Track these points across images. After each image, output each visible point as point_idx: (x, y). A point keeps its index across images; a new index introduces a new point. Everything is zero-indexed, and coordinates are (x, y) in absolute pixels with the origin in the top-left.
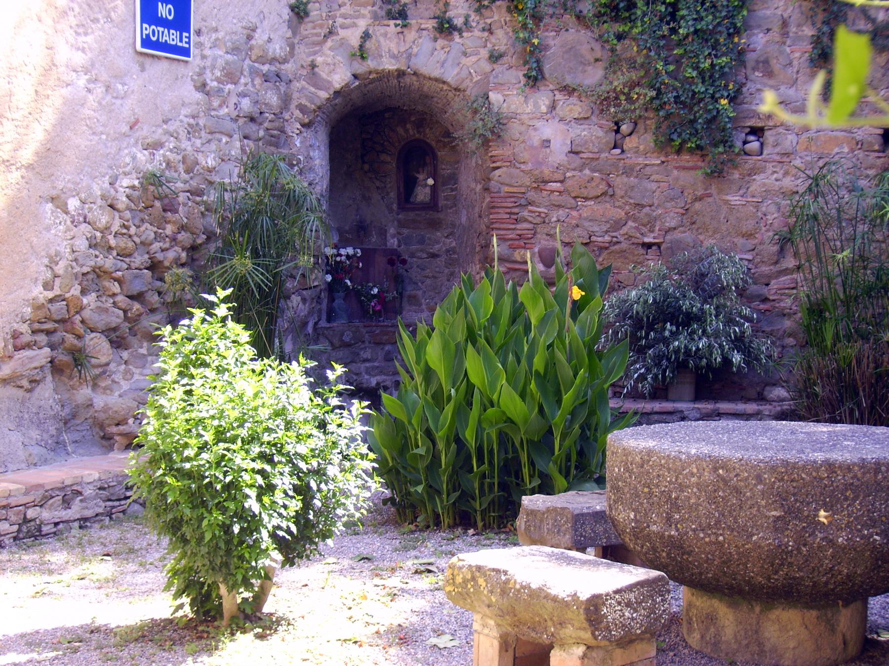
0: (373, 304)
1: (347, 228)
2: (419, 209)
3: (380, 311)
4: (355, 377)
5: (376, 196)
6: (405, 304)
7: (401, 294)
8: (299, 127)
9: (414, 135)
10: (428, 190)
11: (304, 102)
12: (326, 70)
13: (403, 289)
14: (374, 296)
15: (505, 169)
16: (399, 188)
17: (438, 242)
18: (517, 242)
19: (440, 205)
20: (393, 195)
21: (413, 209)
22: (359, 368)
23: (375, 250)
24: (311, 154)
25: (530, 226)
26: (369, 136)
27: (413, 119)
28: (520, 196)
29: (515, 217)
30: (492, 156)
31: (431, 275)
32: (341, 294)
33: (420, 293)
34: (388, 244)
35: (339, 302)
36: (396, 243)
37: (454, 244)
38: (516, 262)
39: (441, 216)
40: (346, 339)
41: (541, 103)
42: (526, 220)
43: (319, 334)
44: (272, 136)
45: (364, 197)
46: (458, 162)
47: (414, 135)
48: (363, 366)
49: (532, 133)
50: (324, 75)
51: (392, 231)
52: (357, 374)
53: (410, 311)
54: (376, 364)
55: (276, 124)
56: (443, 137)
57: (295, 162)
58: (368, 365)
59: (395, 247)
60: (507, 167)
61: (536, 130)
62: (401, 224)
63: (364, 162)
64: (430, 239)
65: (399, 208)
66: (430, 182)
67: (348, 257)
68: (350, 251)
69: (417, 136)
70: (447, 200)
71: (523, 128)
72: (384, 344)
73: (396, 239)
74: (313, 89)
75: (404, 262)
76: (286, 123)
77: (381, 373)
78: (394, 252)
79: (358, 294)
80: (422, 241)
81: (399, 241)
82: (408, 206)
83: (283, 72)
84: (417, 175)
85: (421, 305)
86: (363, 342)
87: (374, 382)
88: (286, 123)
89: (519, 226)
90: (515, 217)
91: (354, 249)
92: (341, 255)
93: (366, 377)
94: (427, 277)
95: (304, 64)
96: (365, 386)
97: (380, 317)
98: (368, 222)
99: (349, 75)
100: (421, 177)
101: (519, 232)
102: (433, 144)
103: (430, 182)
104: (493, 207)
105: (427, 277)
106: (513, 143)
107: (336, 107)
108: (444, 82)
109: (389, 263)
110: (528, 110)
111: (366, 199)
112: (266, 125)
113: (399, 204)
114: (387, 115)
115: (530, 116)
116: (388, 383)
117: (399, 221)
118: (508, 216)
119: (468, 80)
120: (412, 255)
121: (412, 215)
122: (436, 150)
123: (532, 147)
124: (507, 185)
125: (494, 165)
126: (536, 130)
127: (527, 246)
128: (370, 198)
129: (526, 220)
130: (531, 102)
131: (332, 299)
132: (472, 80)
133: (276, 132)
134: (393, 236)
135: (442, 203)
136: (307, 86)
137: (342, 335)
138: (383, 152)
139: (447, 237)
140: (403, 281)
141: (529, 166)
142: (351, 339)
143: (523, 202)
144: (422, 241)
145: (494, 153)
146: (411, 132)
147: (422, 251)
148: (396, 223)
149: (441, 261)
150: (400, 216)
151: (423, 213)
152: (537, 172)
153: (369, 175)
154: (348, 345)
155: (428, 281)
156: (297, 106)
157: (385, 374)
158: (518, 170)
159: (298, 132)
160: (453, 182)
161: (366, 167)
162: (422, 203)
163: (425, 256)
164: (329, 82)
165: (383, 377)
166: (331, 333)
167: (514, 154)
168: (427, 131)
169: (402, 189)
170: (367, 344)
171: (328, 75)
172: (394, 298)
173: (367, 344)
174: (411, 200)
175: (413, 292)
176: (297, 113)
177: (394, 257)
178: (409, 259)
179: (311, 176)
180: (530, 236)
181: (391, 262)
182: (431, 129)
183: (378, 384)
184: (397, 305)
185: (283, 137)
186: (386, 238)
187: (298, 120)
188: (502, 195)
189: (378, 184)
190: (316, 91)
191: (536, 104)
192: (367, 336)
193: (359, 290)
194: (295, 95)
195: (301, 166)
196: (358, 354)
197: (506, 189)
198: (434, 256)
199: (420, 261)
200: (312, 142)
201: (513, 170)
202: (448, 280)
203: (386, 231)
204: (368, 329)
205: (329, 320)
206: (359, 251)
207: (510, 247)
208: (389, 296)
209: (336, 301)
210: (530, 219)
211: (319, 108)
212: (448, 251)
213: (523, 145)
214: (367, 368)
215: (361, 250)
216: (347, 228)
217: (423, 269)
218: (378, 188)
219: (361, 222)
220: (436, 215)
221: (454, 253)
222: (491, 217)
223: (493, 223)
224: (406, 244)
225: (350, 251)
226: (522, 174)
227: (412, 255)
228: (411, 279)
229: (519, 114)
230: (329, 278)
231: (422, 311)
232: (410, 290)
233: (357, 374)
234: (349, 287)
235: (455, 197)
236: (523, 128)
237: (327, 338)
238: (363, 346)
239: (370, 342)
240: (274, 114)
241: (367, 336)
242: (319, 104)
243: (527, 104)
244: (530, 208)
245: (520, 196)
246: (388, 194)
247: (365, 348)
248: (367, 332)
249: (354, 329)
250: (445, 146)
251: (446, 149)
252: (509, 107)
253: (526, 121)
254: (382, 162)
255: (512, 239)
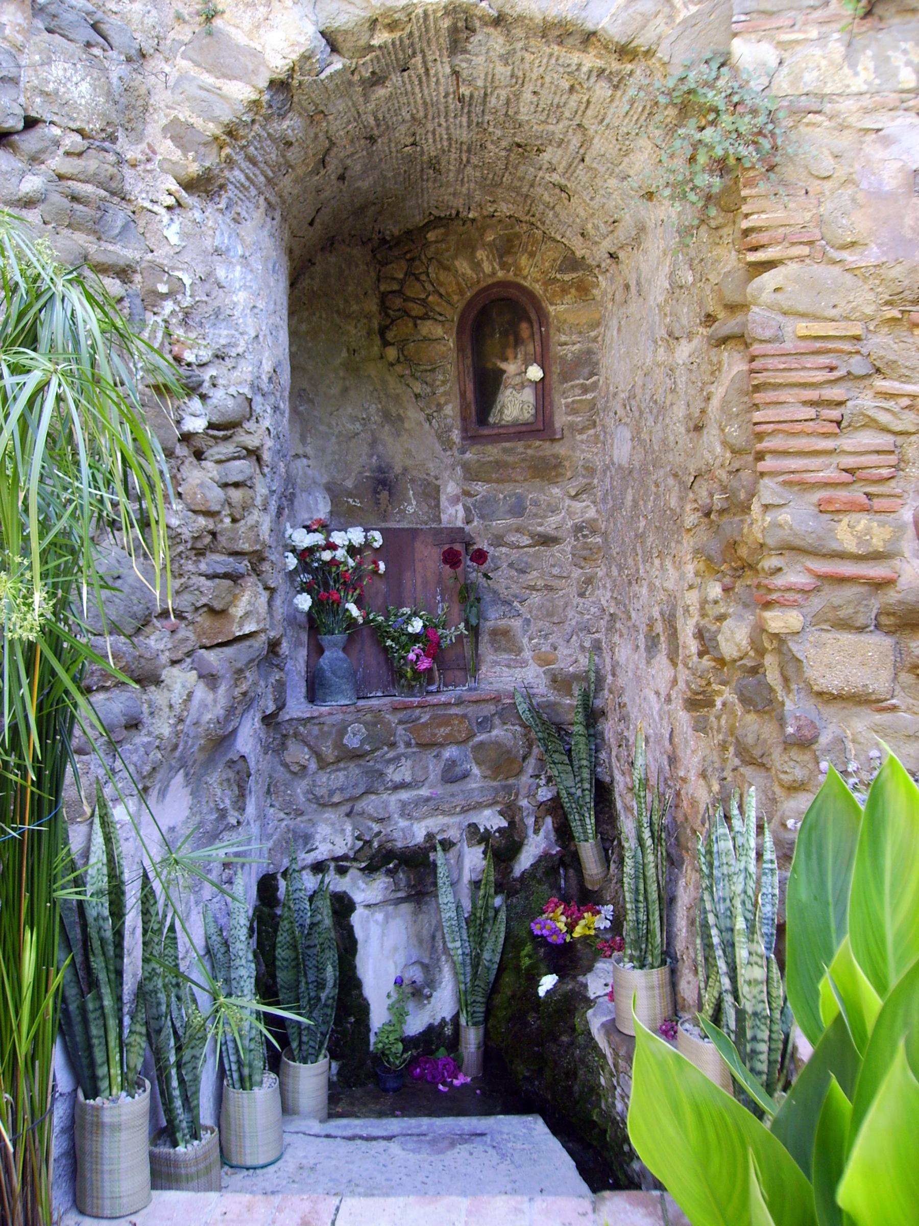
0: (412, 656)
1: (349, 484)
2: (508, 438)
3: (430, 670)
4: (376, 827)
5: (414, 415)
6: (485, 647)
7: (475, 631)
8: (174, 187)
9: (494, 273)
10: (528, 395)
11: (184, 114)
12: (247, 23)
13: (481, 616)
14: (415, 638)
15: (793, 266)
16: (463, 395)
17: (554, 510)
18: (842, 494)
19: (558, 425)
20: (451, 410)
21: (496, 439)
22: (386, 806)
23: (414, 533)
24: (221, 273)
25: (884, 441)
26: (396, 287)
27: (490, 237)
28: (847, 346)
29: (835, 414)
30: (746, 232)
31: (541, 583)
32: (339, 638)
33: (516, 624)
34: (444, 517)
35: (332, 656)
36: (461, 514)
37: (591, 513)
38: (841, 556)
39: (561, 449)
40: (352, 741)
41: (897, 59)
42: (871, 424)
43: (285, 736)
44: (74, 198)
45: (387, 416)
46: (598, 324)
47: (494, 273)
48: (393, 800)
49: (873, 151)
50: (240, 38)
51: (451, 488)
52: (380, 820)
53: (496, 663)
54: (425, 792)
55: (91, 164)
56: (560, 271)
57: (163, 288)
58: (404, 795)
59: (459, 524)
60: (801, 259)
61: (887, 142)
62: (471, 474)
63: (386, 343)
64: (536, 503)
65: (463, 439)
66: (535, 373)
67: (352, 550)
68: (356, 536)
69: (500, 274)
70: (574, 412)
71: (844, 142)
72: (441, 745)
73: (460, 507)
74: (209, 79)
75: (480, 556)
76: (127, 171)
77: (437, 810)
78: (457, 534)
79: (378, 633)
80: (518, 510)
81: (467, 510)
82: (485, 432)
83: (114, 20)
84: (504, 366)
85: (520, 650)
86: (393, 745)
87: (419, 832)
88: (127, 171)
89: (847, 442)
90: (835, 414)
91: (366, 530)
92: (332, 547)
93: (403, 823)
94: (533, 588)
95: (185, 11)
96: (399, 844)
97: (430, 682)
98: (398, 469)
99: (311, 30)
100: (511, 368)
101: (849, 461)
102: (538, 288)
103: (535, 373)
104: (757, 388)
105: (533, 588)
106: (815, 186)
107: (293, 155)
108: (589, 38)
109: (445, 561)
110: (858, 84)
111: (394, 420)
112: (56, 162)
113: (464, 430)
114: (431, 236)
115: (866, 101)
116: (453, 834)
117: (466, 467)
118: (811, 412)
119: (660, 20)
120: (498, 541)
121: (493, 452)
122: (545, 303)
123: (879, 196)
124: (803, 315)
125: (760, 256)
126: (887, 142)
127: (877, 503)
128: (400, 419)
129: (871, 424)
130: (866, 60)
131: (317, 650)
132: (671, 18)
133: (89, 189)
134: (455, 500)
135: (561, 419)
136: (194, 71)
137: (342, 732)
138: (425, 317)
139: (574, 497)
140: (478, 600)
141: (872, 255)
142: (362, 742)
143: (857, 365)
144: (518, 510)
145: (753, 221)
146: (487, 267)
147: (518, 530)
148: (459, 469)
149: (563, 551)
150: (468, 455)
151: (520, 446)
152: (896, 272)
153: (399, 369)
154: (356, 756)
155: (536, 598)
156: (165, 129)
157: (444, 813)
158: (836, 270)
159: (171, 201)
160: (586, 371)
161: (392, 353)
162: (515, 424)
163: (526, 540)
164: (255, 54)
165: (442, 820)
166: (316, 730)
167: (821, 221)
168: (524, 260)
169: (470, 396)
170: (402, 749)
171: (249, 34)
172: (460, 637)
173: (402, 749)
174: (491, 420)
175: (502, 623)
176: (167, 148)
177: (458, 547)
178: (491, 551)
179: (221, 336)
180: (885, 472)
181: (451, 559)
182: (532, 255)
183: (430, 836)
184: (468, 650)
185: (118, 216)
186: (438, 505)
187: (168, 167)
188: (788, 346)
189: (418, 388)
190: (219, 83)
191: (883, 66)
192: (400, 730)
193: (379, 626)
194: (161, 98)
195: (187, 301)
196: (381, 774)
197: (803, 327)
198: (547, 540)
199: (515, 554)
200: (222, 240)
201: (821, 271)
202: (582, 595)
203: (437, 489)
204: (402, 715)
205: (312, 697)
206: (377, 535)
207: (822, 508)
208: (449, 634)
209: (327, 653)
210: (884, 418)
211: (231, 133)
212: (578, 529)
213: (849, 190)
214: (404, 805)
215: (383, 531)
216: (349, 484)
217: (523, 572)
218: (417, 396)
219: (380, 470)
220: (549, 449)
221: (594, 532)
222: (757, 416)
223: (760, 436)
224: (482, 517)
225: (356, 536)
226: (848, 276)
227: (498, 541)
228: (495, 592)
229: (831, 97)
230: (304, 602)
231: (524, 664)
232: (494, 618)
233: (380, 820)
234: (355, 619)
235: (593, 405)
236: (844, 142)
237: (306, 743)
238: (391, 755)
239: (408, 745)
240: (79, 131)
241: (400, 730)
242: (227, 117)
243: (853, 66)
244: (881, 384)
245: (847, 346)
246: (440, 408)
247: (397, 759)
248: (401, 722)
249: (369, 717)
250: (564, 291)
251: (568, 298)
252: (796, 79)
253: (852, 120)
254: (426, 339)
255: (826, 485)
